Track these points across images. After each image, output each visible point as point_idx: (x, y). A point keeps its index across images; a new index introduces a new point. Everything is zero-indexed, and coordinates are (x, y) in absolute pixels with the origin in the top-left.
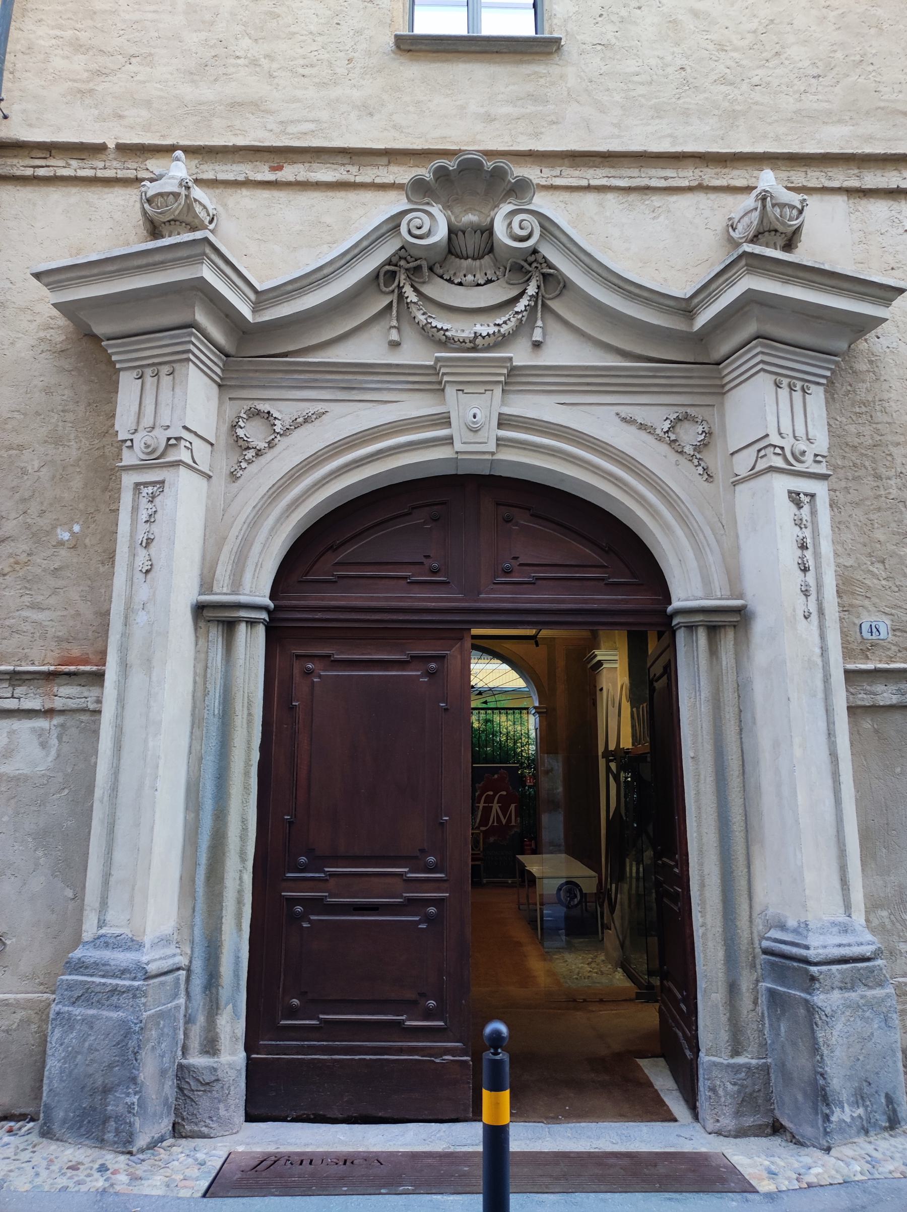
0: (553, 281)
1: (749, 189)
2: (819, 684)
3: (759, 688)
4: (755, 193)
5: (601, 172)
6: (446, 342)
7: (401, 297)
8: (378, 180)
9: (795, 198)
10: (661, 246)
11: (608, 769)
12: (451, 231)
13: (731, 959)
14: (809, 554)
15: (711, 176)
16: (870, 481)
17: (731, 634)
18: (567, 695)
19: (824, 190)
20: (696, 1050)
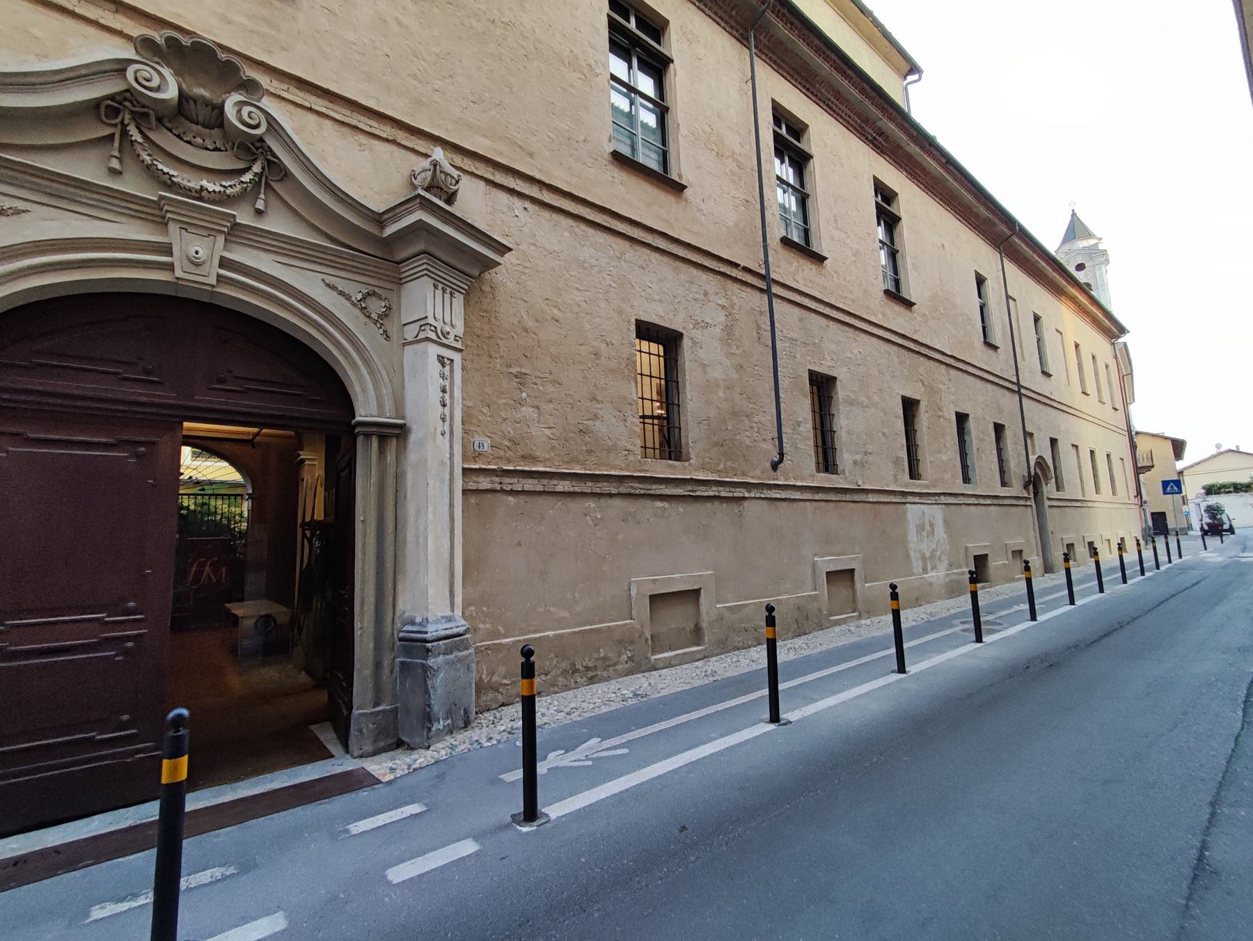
0: (273, 165)
1: (427, 156)
2: (447, 477)
3: (410, 477)
4: (430, 160)
5: (320, 101)
6: (172, 186)
7: (125, 133)
8: (101, 21)
9: (455, 173)
10: (369, 174)
11: (304, 535)
12: (182, 94)
13: (378, 647)
14: (447, 396)
15: (401, 136)
16: (486, 358)
17: (394, 442)
18: (271, 477)
19: (472, 174)
20: (350, 709)
